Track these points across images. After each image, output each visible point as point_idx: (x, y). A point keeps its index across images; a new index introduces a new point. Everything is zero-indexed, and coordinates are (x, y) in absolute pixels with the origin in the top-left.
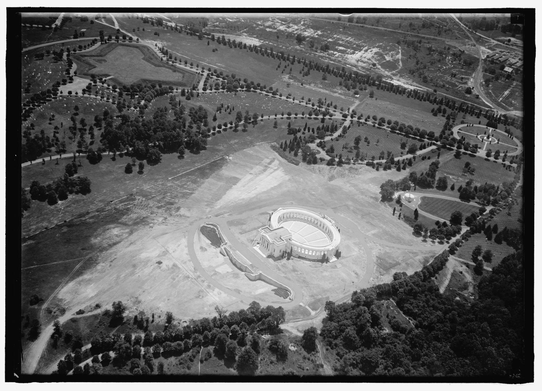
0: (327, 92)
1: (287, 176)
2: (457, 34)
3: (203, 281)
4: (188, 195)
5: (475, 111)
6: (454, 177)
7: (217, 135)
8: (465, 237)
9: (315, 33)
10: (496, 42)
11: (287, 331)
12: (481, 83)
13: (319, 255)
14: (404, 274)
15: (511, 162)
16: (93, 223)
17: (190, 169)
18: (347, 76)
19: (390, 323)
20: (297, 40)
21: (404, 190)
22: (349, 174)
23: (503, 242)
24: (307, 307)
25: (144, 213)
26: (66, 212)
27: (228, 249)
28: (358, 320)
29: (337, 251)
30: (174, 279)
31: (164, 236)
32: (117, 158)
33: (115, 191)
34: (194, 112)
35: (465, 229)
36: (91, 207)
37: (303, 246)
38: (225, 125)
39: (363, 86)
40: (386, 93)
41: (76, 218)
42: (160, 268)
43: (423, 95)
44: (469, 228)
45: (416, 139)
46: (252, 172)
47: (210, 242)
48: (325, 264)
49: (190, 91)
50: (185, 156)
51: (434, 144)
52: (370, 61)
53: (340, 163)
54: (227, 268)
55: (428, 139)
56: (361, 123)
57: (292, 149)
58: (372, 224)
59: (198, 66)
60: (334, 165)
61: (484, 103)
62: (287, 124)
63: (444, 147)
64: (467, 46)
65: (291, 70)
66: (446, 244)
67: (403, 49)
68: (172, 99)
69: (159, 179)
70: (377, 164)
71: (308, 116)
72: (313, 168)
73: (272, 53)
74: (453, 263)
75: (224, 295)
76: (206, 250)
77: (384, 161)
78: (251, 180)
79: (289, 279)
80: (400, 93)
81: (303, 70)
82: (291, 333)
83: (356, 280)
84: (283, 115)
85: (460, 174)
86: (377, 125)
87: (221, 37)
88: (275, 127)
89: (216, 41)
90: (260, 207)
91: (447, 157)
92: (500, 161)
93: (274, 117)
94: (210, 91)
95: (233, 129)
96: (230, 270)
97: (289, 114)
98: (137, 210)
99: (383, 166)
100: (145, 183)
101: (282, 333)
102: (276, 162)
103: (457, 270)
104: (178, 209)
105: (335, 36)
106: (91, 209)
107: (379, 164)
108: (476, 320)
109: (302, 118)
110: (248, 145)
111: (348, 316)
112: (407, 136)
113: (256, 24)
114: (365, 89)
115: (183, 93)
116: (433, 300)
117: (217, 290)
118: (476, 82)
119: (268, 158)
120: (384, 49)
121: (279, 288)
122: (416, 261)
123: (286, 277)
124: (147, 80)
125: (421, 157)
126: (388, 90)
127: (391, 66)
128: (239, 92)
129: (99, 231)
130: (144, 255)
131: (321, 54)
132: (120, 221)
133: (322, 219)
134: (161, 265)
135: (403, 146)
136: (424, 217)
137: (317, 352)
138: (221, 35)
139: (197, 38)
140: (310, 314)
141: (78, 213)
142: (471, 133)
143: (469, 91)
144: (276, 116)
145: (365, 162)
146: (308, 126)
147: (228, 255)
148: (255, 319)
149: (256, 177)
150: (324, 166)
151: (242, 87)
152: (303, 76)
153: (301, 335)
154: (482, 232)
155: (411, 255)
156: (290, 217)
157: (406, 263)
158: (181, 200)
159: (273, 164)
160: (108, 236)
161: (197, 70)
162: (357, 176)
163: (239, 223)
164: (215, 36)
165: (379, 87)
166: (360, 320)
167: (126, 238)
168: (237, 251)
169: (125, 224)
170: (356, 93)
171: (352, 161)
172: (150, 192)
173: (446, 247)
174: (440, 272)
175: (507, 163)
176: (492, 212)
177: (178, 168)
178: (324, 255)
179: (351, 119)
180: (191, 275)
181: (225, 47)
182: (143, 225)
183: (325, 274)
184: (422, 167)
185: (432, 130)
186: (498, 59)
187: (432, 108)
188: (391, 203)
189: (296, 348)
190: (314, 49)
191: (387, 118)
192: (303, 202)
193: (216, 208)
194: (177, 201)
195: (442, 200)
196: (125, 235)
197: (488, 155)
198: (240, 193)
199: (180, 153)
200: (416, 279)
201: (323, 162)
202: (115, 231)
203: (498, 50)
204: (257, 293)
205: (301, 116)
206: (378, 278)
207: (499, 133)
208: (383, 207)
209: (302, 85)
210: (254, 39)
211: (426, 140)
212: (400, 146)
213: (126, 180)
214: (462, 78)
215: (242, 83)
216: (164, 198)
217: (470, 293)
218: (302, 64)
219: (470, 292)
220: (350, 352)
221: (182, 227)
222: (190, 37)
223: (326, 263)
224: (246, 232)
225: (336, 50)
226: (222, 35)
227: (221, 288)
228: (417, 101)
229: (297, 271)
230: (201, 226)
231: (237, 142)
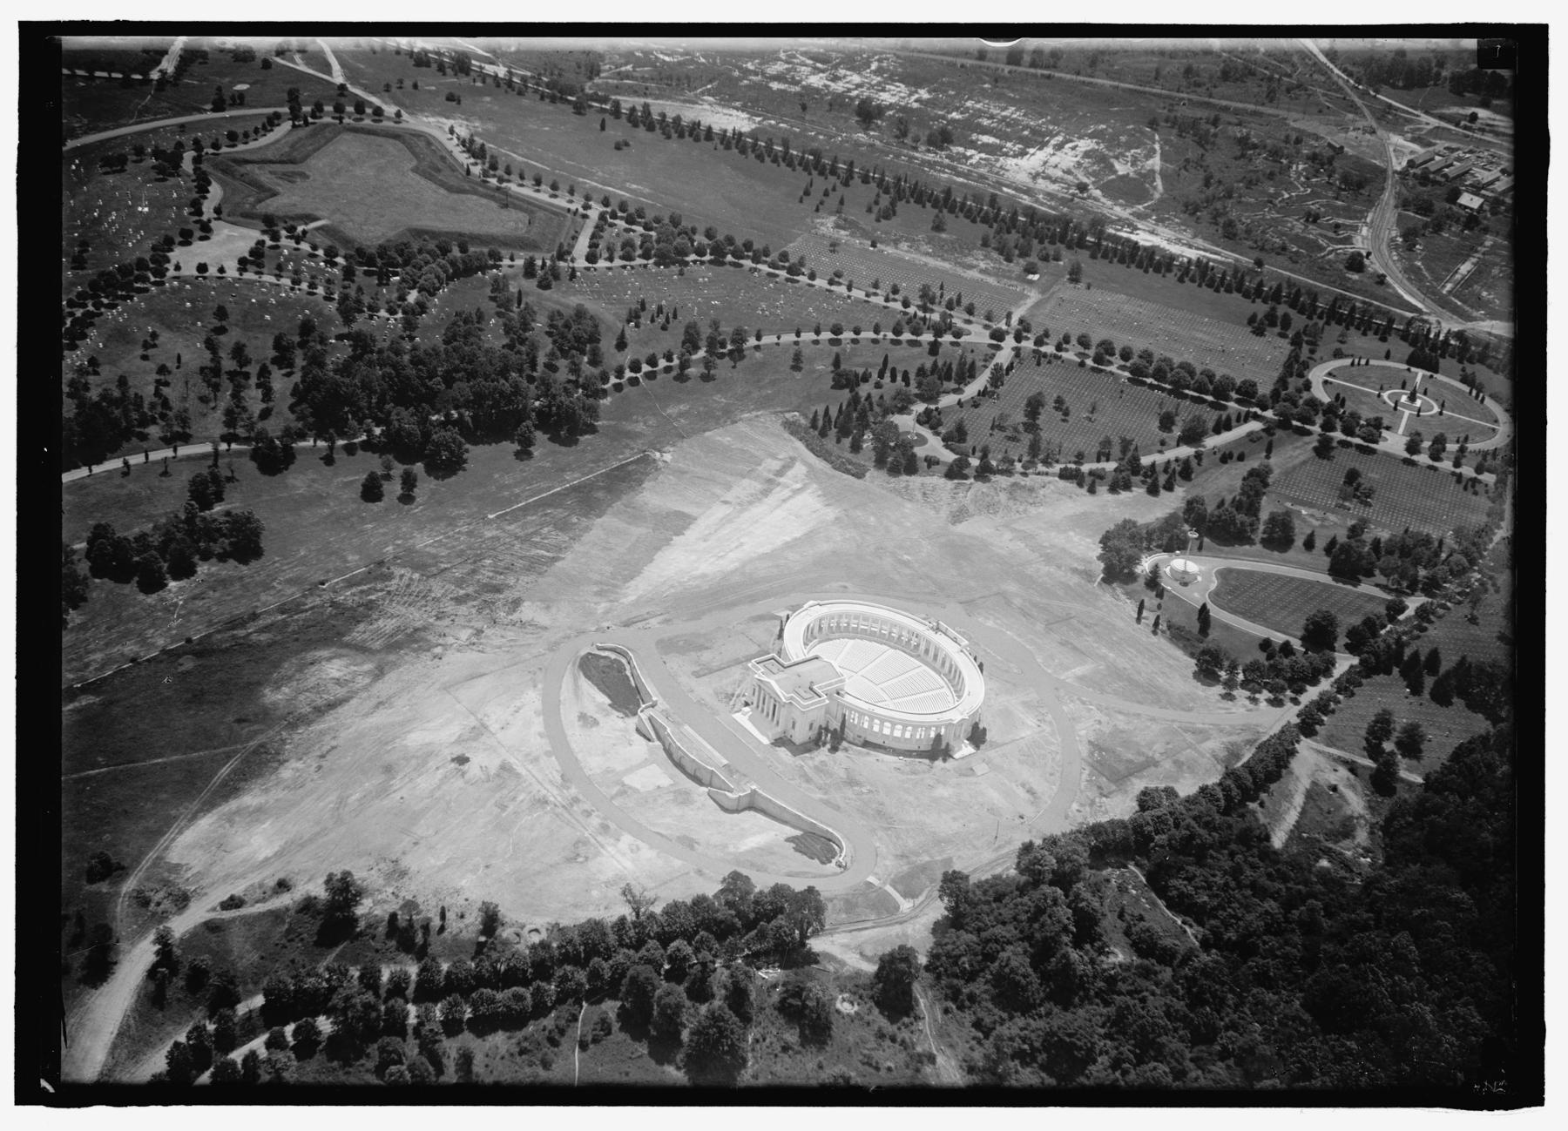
0: (947, 265)
1: (829, 510)
2: (1322, 99)
3: (588, 814)
4: (545, 564)
5: (1373, 322)
6: (1312, 511)
7: (627, 389)
8: (1347, 686)
9: (911, 94)
10: (1434, 122)
11: (831, 958)
12: (1393, 240)
13: (924, 738)
14: (1170, 792)
16: (269, 645)
17: (549, 489)
18: (1003, 220)
19: (1127, 933)
20: (859, 114)
21: (1169, 549)
22: (1011, 503)
23: (1455, 700)
24: (889, 888)
25: (416, 616)
26: (191, 612)
27: (661, 720)
28: (1036, 926)
29: (975, 726)
30: (503, 808)
31: (475, 682)
32: (339, 456)
33: (333, 553)
34: (560, 323)
35: (1344, 663)
36: (263, 597)
37: (877, 710)
38: (652, 361)
39: (1051, 249)
40: (1117, 269)
41: (219, 632)
42: (463, 775)
43: (1224, 274)
44: (1356, 661)
45: (1204, 401)
46: (729, 497)
47: (608, 701)
48: (939, 763)
49: (548, 263)
50: (536, 452)
51: (1256, 417)
52: (1070, 178)
53: (984, 473)
54: (656, 776)
55: (1238, 401)
56: (1045, 355)
58: (1075, 648)
59: (571, 192)
60: (966, 477)
61: (1401, 297)
62: (831, 360)
63: (1284, 424)
64: (1352, 134)
65: (842, 202)
66: (1289, 705)
67: (1165, 142)
68: (498, 286)
69: (460, 517)
70: (1091, 473)
71: (890, 335)
72: (906, 487)
74: (1311, 762)
75: (647, 853)
76: (596, 723)
77: (1111, 466)
78: (727, 520)
79: (838, 808)
80: (1157, 270)
81: (876, 203)
82: (842, 963)
83: (1029, 811)
84: (818, 332)
85: (1332, 503)
86: (1089, 362)
87: (639, 108)
88: (796, 367)
89: (624, 119)
90: (753, 599)
91: (1292, 454)
92: (1446, 465)
93: (792, 337)
94: (608, 264)
95: (674, 373)
96: (665, 782)
97: (837, 330)
98: (397, 608)
99: (1109, 479)
100: (421, 530)
101: (817, 962)
102: (799, 469)
103: (1322, 782)
104: (516, 603)
105: (969, 104)
106: (264, 604)
107: (1097, 476)
108: (1377, 927)
109: (875, 341)
110: (718, 418)
111: (1007, 913)
112: (1177, 392)
113: (740, 68)
114: (1057, 259)
115: (529, 270)
116: (1253, 867)
117: (627, 839)
118: (1376, 237)
119: (774, 457)
120: (1112, 142)
121: (806, 833)
122: (1203, 756)
123: (827, 803)
124: (427, 232)
126: (1121, 261)
127: (1131, 190)
128: (692, 267)
129: (288, 667)
130: (415, 739)
131: (930, 157)
132: (346, 639)
133: (931, 635)
134: (466, 767)
135: (1167, 422)
136: (1227, 627)
137: (917, 1018)
138: (638, 102)
139: (570, 109)
140: (897, 908)
141: (225, 617)
142: (1363, 385)
144: (798, 335)
145: (1057, 468)
146: (890, 366)
147: (659, 738)
148: (739, 924)
149: (741, 512)
150: (937, 481)
151: (700, 252)
152: (878, 220)
153: (871, 968)
154: (1396, 670)
155: (1189, 737)
156: (838, 626)
157: (1175, 762)
158: (524, 579)
159: (790, 473)
160: (312, 681)
161: (571, 202)
162: (1033, 510)
163: (692, 645)
164: (623, 105)
165: (1096, 251)
166: (1043, 925)
167: (366, 688)
168: (686, 727)
169: (361, 649)
170: (1031, 270)
171: (1018, 466)
172: (435, 557)
173: (1289, 714)
174: (1273, 786)
175: (1467, 471)
176: (1423, 613)
177: (516, 485)
178: (938, 737)
179: (1015, 344)
180: (554, 794)
181: (650, 135)
182: (415, 650)
183: (941, 791)
184: (1222, 484)
186: (1440, 170)
187: (1249, 313)
188: (1130, 587)
189: (856, 1008)
190: (908, 141)
191: (1121, 340)
192: (878, 586)
193: (624, 600)
194: (511, 581)
195: (1279, 578)
196: (362, 681)
197: (1413, 447)
198: (693, 557)
199: (520, 443)
200: (1204, 806)
201: (935, 468)
202: (334, 668)
203: (1441, 145)
204: (743, 848)
205: (872, 335)
206: (1092, 803)
207: (1444, 385)
208: (1108, 597)
209: (874, 245)
210: (735, 112)
211: (1231, 404)
212: (1157, 423)
213: (363, 520)
214: (1337, 226)
215: (700, 239)
216: (474, 572)
217: (1359, 848)
218: (873, 185)
219: (1359, 845)
220: (1011, 1018)
221: (527, 656)
222: (551, 108)
223: (945, 760)
224: (711, 671)
225: (973, 145)
226: (642, 100)
227: (639, 832)
228: (1207, 292)
229: (858, 784)
230: (583, 653)
231: (687, 412)
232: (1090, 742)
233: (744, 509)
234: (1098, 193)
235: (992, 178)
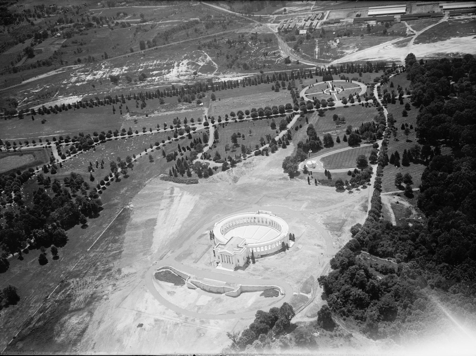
0: (173, 112)
1: (195, 197)
3: (194, 320)
5: (304, 74)
6: (332, 131)
7: (103, 192)
9: (122, 69)
10: (276, 16)
11: (300, 323)
12: (291, 51)
13: (278, 245)
14: (359, 225)
15: (367, 100)
17: (101, 233)
18: (180, 92)
19: (377, 270)
20: (112, 81)
22: (247, 169)
23: (410, 163)
25: (89, 291)
26: (8, 328)
28: (355, 280)
29: (290, 235)
30: (166, 332)
31: (126, 299)
33: (43, 286)
34: (69, 181)
35: (375, 168)
36: (30, 311)
37: (261, 244)
38: (107, 179)
39: (201, 93)
40: (224, 92)
41: (23, 330)
42: (145, 329)
43: (255, 79)
44: (377, 165)
45: (278, 116)
46: (161, 207)
48: (287, 251)
50: (88, 224)
51: (296, 114)
52: (189, 73)
54: (206, 298)
55: (287, 112)
56: (223, 124)
57: (182, 173)
58: (298, 200)
59: (41, 141)
60: (229, 168)
61: (306, 65)
62: (161, 154)
63: (305, 112)
64: (256, 28)
65: (127, 108)
66: (368, 186)
67: (207, 52)
69: (78, 255)
70: (264, 150)
71: (174, 139)
72: (213, 179)
73: (87, 103)
74: (387, 199)
75: (221, 322)
77: (267, 145)
78: (167, 215)
79: (269, 278)
80: (235, 87)
81: (138, 103)
82: (305, 322)
83: (322, 251)
84: (152, 148)
85: (335, 127)
86: (238, 120)
87: (41, 108)
88: (152, 161)
89: (38, 114)
90: (194, 233)
91: (314, 119)
92: (356, 103)
94: (69, 157)
95: (115, 180)
96: (210, 298)
97: (157, 144)
99: (270, 149)
100: (68, 265)
101: (297, 326)
102: (176, 190)
103: (393, 203)
104: (119, 271)
105: (141, 65)
106: (32, 313)
107: (266, 150)
109: (170, 143)
111: (342, 281)
113: (63, 84)
114: (204, 96)
115: (45, 170)
116: (396, 234)
117: (212, 321)
118: (286, 52)
119: (166, 190)
120: (192, 58)
121: (265, 290)
122: (357, 212)
123: (264, 279)
125: (294, 129)
126: (223, 89)
127: (208, 68)
128: (96, 147)
129: (57, 327)
130: (120, 327)
131: (143, 84)
132: (70, 309)
133: (257, 216)
134: (143, 327)
135: (273, 126)
136: (335, 174)
137: (338, 326)
139: (18, 118)
140: (307, 298)
141: (22, 324)
142: (317, 92)
143: (287, 61)
144: (146, 151)
145: (253, 153)
146: (181, 148)
147: (198, 287)
148: (268, 326)
149: (170, 208)
150: (221, 173)
151: (96, 141)
152: (142, 109)
154: (389, 163)
155: (349, 208)
156: (230, 226)
157: (351, 217)
158: (115, 263)
159: (175, 192)
161: (42, 145)
163: (187, 254)
164: (35, 110)
165: (213, 89)
167: (90, 320)
168: (205, 279)
169: (78, 310)
170: (199, 102)
171: (242, 158)
172: (79, 271)
173: (369, 191)
174: (382, 210)
175: (364, 102)
176: (384, 144)
177: (89, 236)
179: (213, 125)
180: (178, 320)
182: (97, 301)
184: (302, 136)
185: (287, 103)
187: (271, 87)
188: (300, 176)
189: (319, 333)
190: (133, 82)
191: (243, 110)
192: (228, 211)
194: (111, 265)
195: (338, 154)
196: (87, 319)
197: (345, 102)
198: (165, 230)
199: (82, 223)
200: (371, 225)
201: (217, 170)
202: (73, 321)
203: (282, 21)
204: (249, 305)
205: (168, 141)
206: (338, 240)
208: (296, 182)
209: (147, 116)
210: (72, 97)
211: (286, 113)
212: (270, 128)
214: (274, 53)
216: (96, 269)
218: (132, 99)
219: (415, 215)
220: (365, 311)
221: (136, 284)
222: (11, 121)
223: (288, 249)
224: (199, 259)
225: (153, 76)
226: (41, 105)
227: (214, 317)
228: (253, 87)
229: (269, 269)
230: (154, 274)
231: (128, 189)
232: (324, 224)
233: (167, 210)
234: (200, 73)
235: (166, 82)
